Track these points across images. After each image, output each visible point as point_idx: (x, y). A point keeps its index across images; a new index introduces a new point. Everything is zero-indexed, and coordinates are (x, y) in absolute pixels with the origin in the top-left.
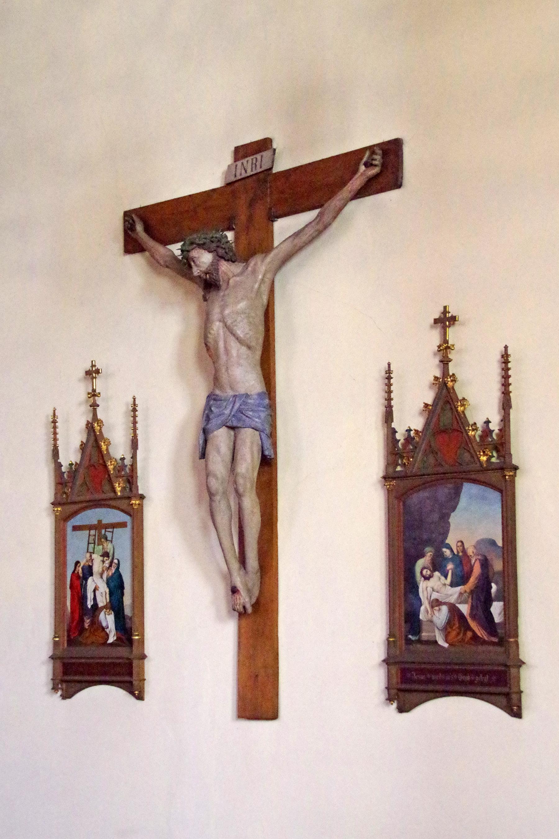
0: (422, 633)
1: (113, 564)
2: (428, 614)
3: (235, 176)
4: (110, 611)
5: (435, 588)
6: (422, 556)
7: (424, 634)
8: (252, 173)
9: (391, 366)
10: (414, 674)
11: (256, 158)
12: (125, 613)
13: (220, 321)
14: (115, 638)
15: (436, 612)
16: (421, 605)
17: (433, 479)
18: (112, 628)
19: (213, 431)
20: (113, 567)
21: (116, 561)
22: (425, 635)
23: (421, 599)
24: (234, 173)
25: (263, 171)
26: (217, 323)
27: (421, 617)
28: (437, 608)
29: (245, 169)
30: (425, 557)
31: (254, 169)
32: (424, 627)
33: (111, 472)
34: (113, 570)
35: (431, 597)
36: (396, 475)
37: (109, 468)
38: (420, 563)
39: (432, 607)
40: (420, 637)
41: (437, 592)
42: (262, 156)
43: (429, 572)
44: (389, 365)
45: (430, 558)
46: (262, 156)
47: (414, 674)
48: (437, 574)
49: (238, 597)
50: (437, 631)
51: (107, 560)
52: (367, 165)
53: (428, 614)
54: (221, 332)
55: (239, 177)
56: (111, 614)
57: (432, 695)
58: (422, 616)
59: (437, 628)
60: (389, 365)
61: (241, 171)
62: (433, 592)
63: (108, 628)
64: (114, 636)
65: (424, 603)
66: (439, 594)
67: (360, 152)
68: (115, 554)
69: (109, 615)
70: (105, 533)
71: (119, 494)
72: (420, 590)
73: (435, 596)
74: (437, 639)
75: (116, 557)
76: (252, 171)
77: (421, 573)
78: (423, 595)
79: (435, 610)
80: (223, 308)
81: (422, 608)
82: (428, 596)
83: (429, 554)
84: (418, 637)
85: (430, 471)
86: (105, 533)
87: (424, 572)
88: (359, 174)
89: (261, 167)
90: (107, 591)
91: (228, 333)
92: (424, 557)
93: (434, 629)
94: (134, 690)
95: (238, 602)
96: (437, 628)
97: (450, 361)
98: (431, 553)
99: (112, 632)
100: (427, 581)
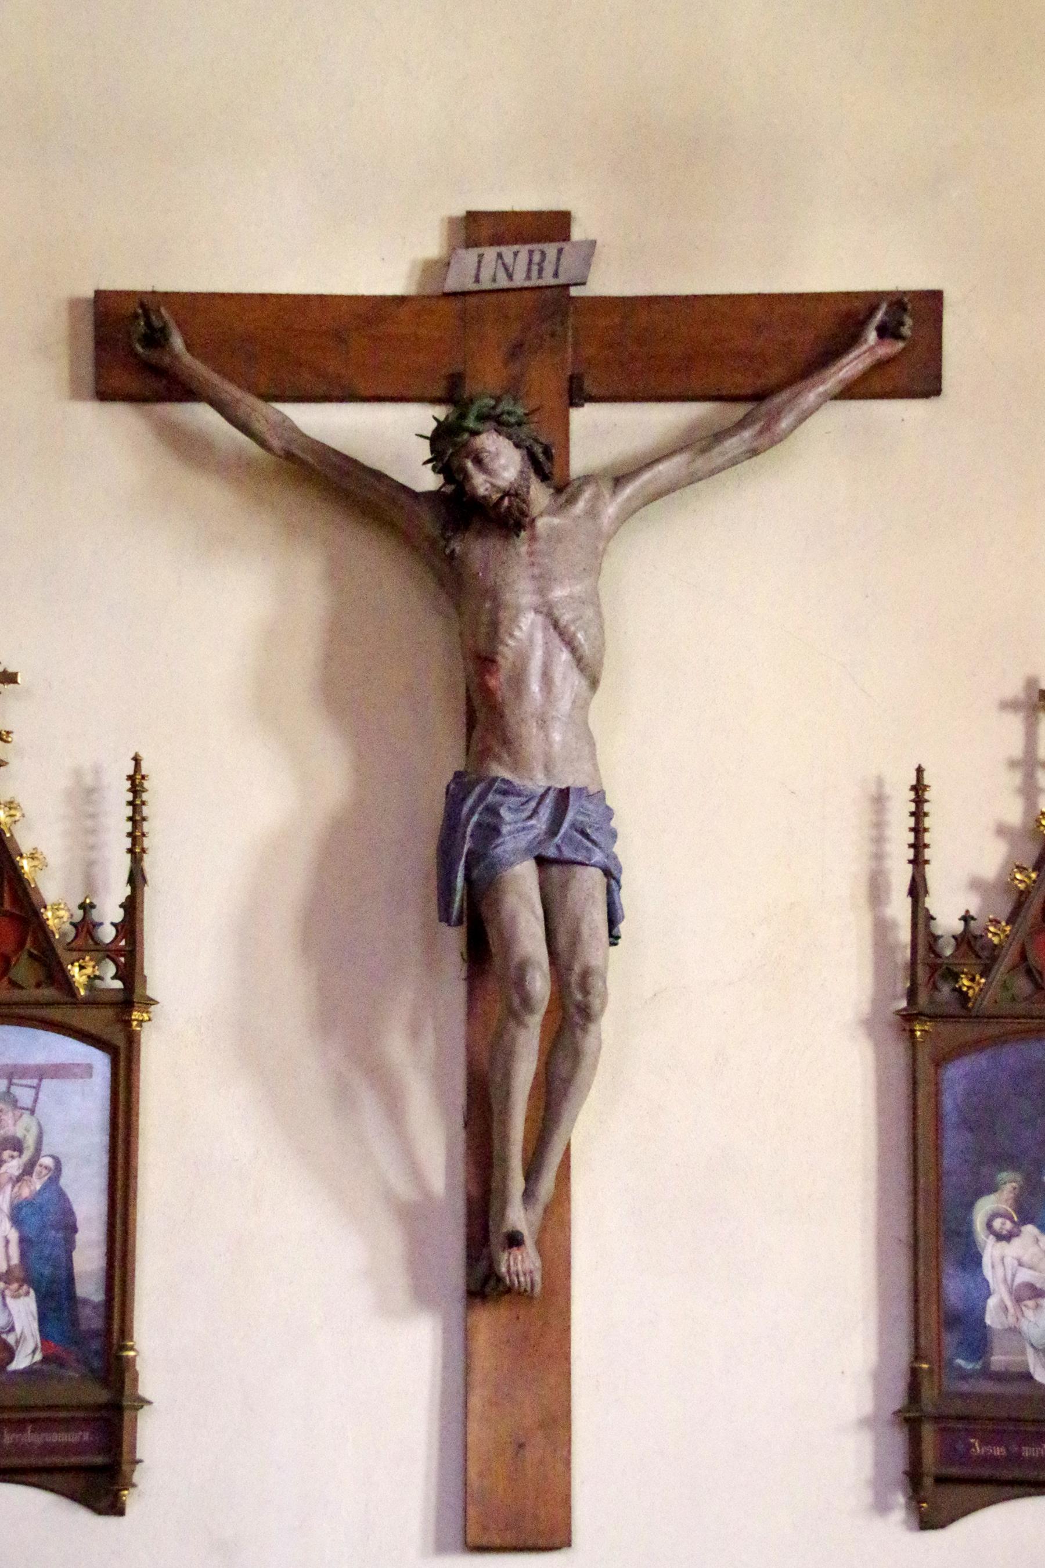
0: (992, 1355)
1: (37, 1168)
2: (1006, 1315)
3: (477, 280)
4: (21, 1286)
5: (1026, 1259)
6: (991, 1188)
7: (994, 1358)
8: (527, 284)
9: (926, 774)
10: (977, 1444)
11: (543, 254)
12: (78, 1295)
13: (537, 611)
14: (38, 1357)
15: (1029, 1313)
16: (989, 1294)
17: (1031, 1025)
18: (27, 1333)
19: (512, 864)
20: (34, 1174)
21: (47, 1161)
22: (998, 1360)
23: (987, 1282)
24: (473, 272)
25: (558, 286)
26: (531, 616)
27: (988, 1321)
28: (1030, 1303)
29: (506, 269)
30: (999, 1191)
31: (535, 273)
32: (997, 1344)
33: (54, 936)
34: (37, 1183)
35: (1013, 1281)
36: (938, 1011)
37: (48, 925)
38: (985, 1207)
39: (1018, 1300)
40: (986, 1366)
41: (1031, 1268)
42: (560, 251)
43: (1009, 1225)
44: (920, 771)
45: (1012, 1195)
46: (560, 251)
47: (977, 1444)
48: (1030, 1229)
49: (520, 1257)
50: (1030, 1351)
51: (12, 1157)
52: (883, 332)
53: (1006, 1315)
54: (539, 637)
55: (486, 284)
56: (27, 1294)
57: (987, 1491)
58: (992, 1318)
59: (1032, 1345)
60: (920, 771)
61: (495, 273)
62: (1020, 1268)
63: (12, 1329)
64: (34, 1352)
65: (997, 1289)
66: (1037, 1274)
67: (871, 300)
68: (46, 1140)
69: (16, 1296)
70: (9, 1088)
71: (82, 992)
72: (986, 1261)
73: (1024, 1276)
74: (1032, 1371)
75: (46, 1150)
76: (528, 277)
77: (989, 1226)
78: (994, 1273)
79: (1025, 1305)
80: (543, 582)
81: (992, 1302)
82: (1005, 1275)
83: (1009, 1187)
84: (980, 1363)
85: (1020, 1008)
86: (9, 1088)
87: (997, 1224)
88: (865, 347)
89: (556, 275)
90: (14, 1235)
91: (557, 641)
92: (996, 1191)
93: (1024, 1348)
94: (120, 1488)
95: (519, 1266)
96: (1032, 1345)
97: (144, 792)
98: (1014, 1184)
99: (25, 1339)
100: (1004, 1243)
